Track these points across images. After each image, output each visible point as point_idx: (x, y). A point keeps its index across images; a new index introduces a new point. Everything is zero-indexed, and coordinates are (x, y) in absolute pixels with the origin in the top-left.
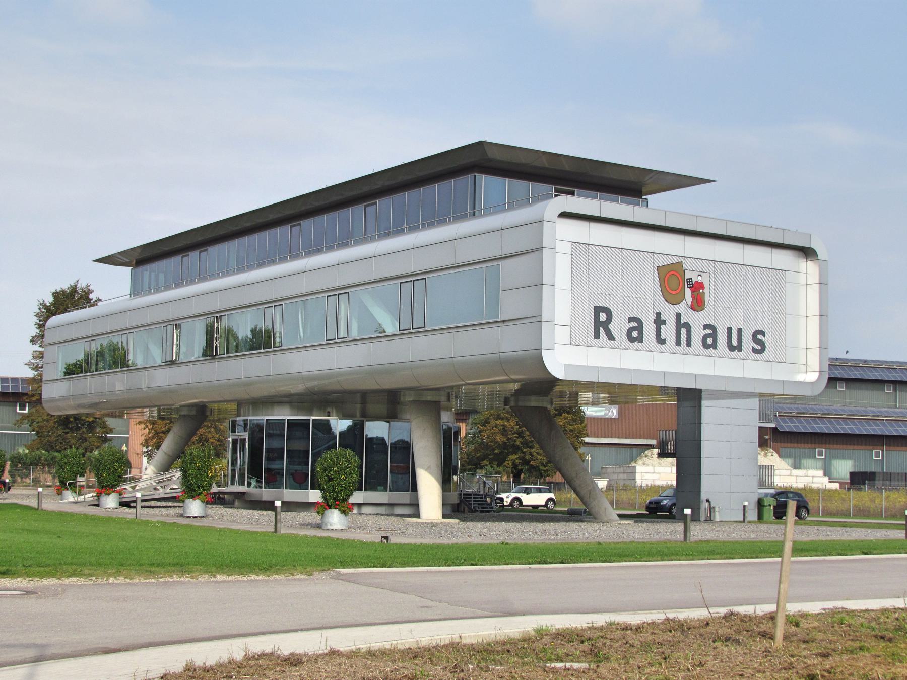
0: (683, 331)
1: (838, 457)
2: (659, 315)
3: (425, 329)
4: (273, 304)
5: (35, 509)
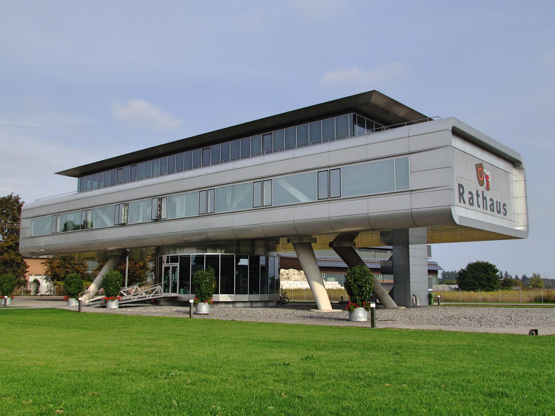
1: (330, 277)
3: (341, 198)
4: (262, 180)
5: (76, 311)
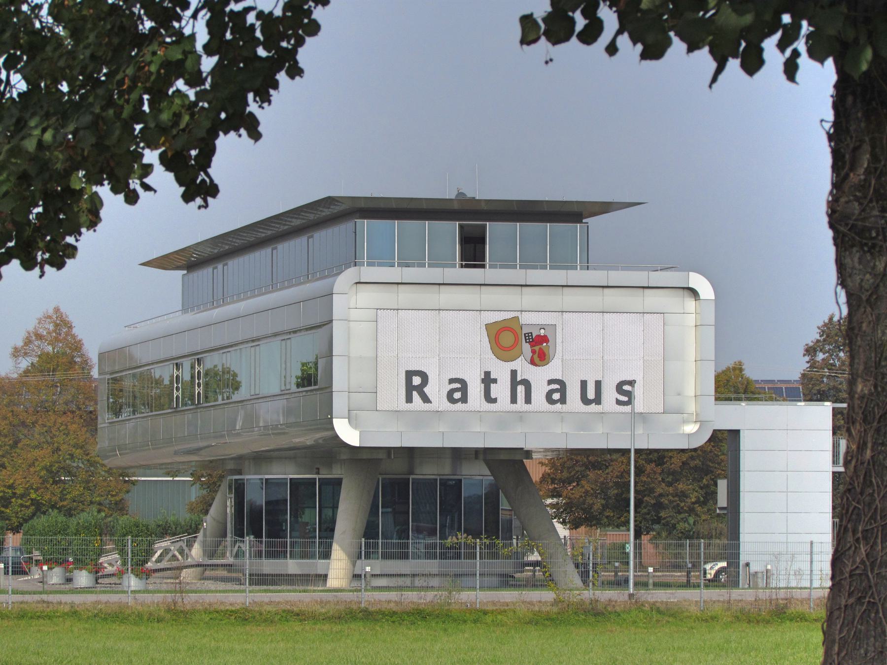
0: (521, 389)
2: (487, 374)
